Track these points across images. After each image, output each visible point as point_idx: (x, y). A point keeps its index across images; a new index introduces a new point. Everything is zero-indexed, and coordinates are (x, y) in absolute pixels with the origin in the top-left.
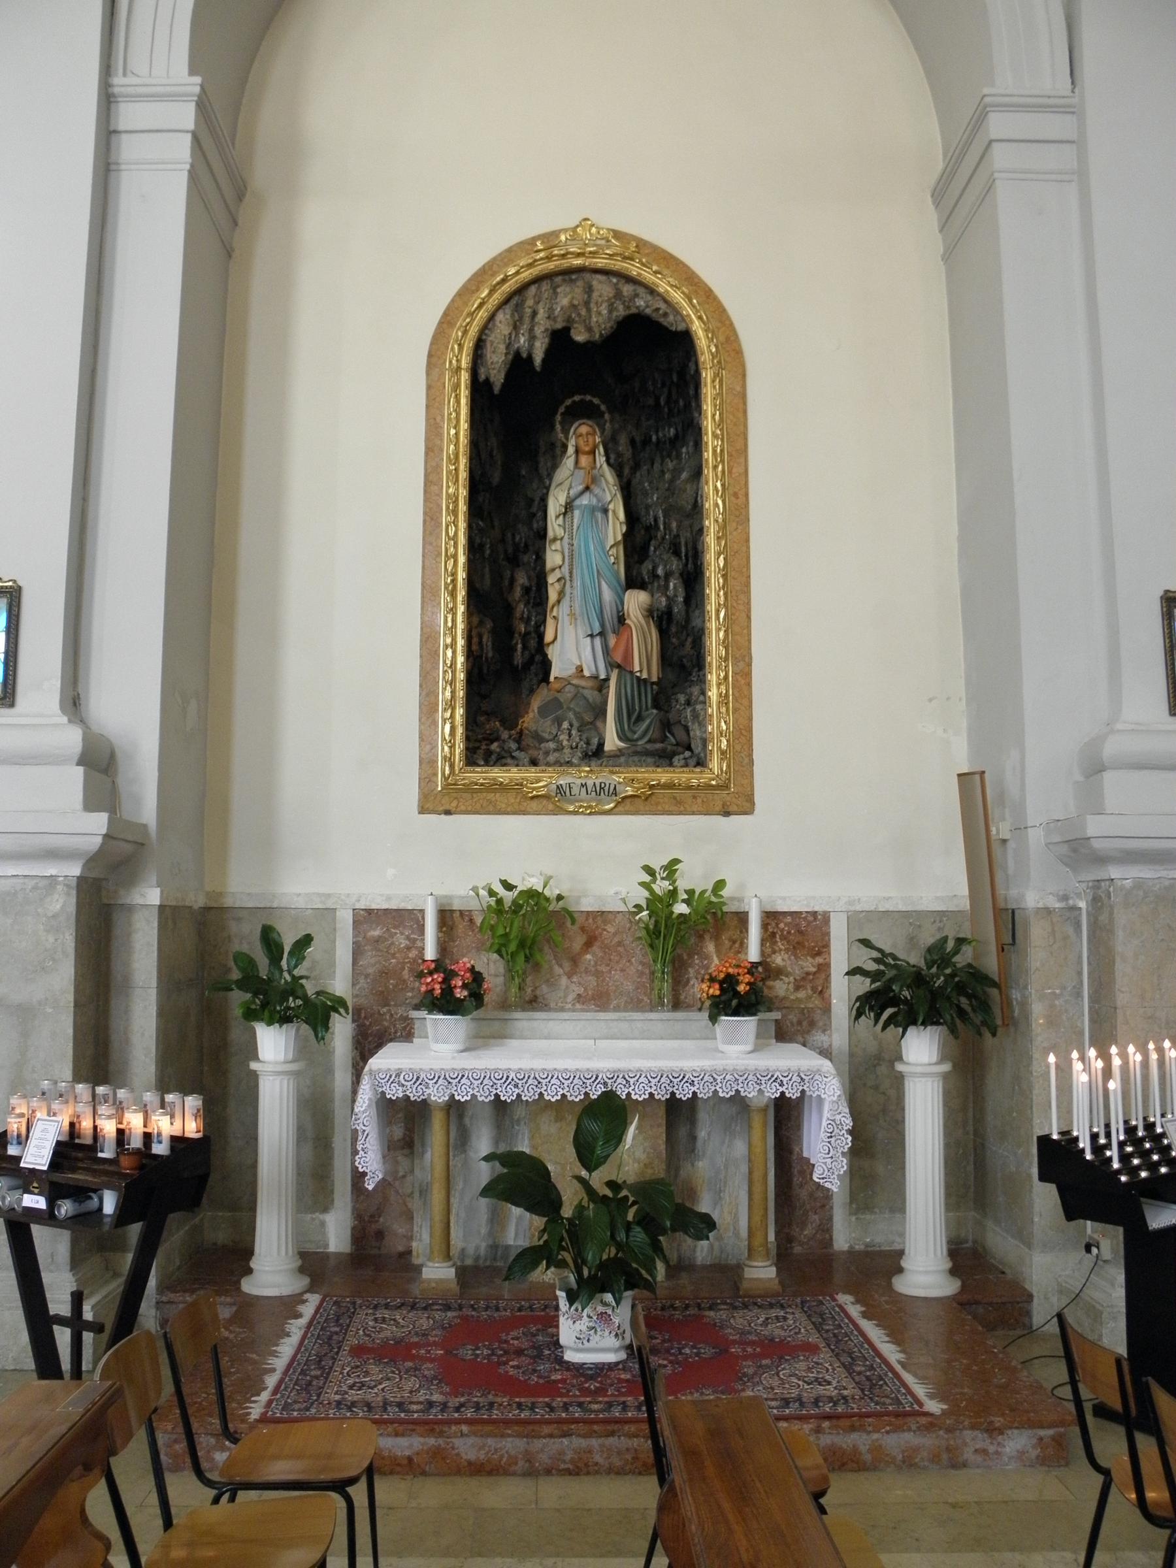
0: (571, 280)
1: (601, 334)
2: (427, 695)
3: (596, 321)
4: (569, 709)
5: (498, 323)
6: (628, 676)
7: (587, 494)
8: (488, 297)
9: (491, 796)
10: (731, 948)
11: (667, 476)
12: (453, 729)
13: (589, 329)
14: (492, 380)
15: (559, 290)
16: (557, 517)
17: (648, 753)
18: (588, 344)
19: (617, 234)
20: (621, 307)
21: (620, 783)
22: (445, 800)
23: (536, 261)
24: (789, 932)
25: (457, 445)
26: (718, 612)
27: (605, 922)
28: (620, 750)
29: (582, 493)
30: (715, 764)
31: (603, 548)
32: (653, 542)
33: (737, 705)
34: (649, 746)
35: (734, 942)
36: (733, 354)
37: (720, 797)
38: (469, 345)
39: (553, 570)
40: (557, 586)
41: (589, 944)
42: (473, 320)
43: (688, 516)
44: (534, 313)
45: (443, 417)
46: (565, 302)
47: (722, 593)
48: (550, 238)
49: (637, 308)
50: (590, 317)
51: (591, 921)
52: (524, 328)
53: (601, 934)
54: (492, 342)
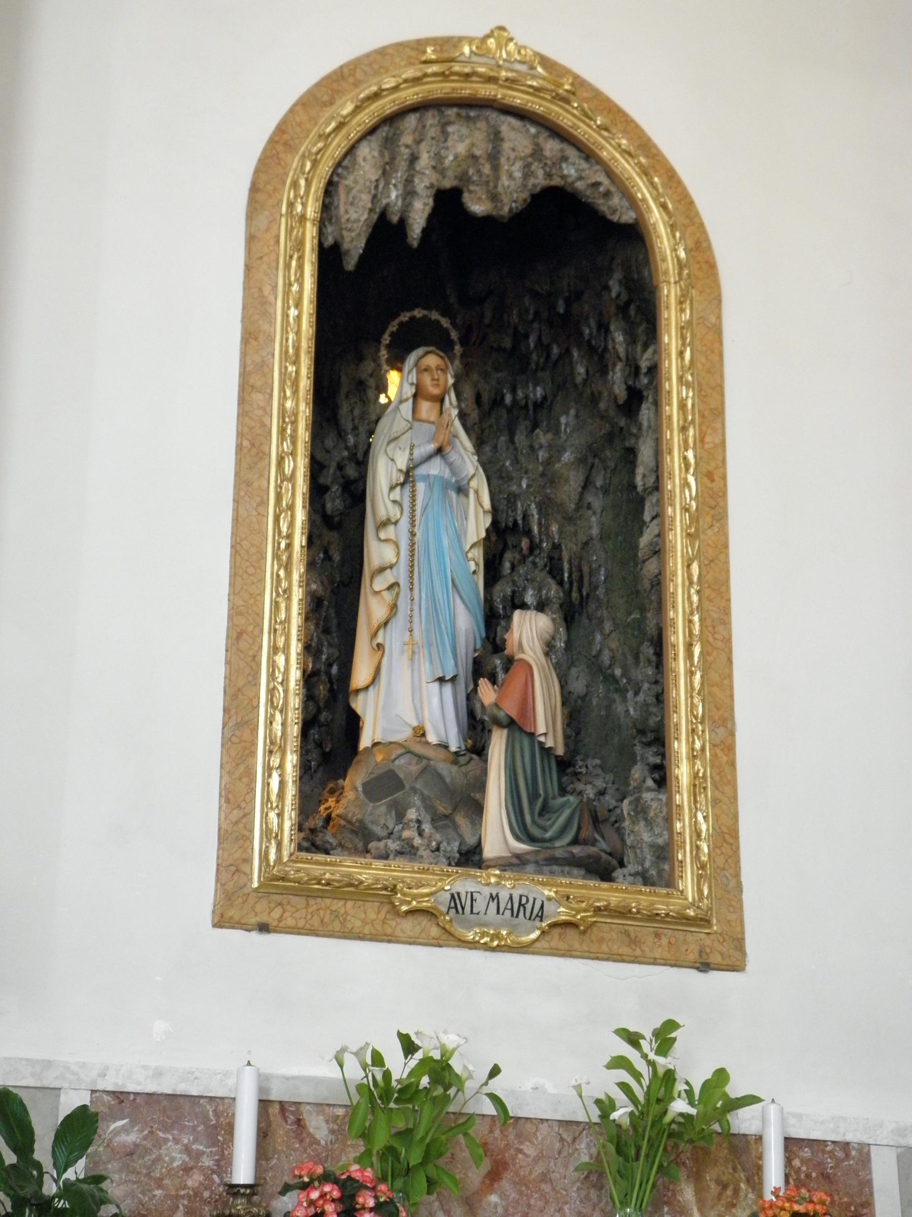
0: (468, 118)
1: (511, 209)
2: (238, 726)
3: (503, 189)
4: (414, 790)
5: (360, 159)
6: (526, 742)
7: (437, 461)
8: (352, 113)
9: (338, 905)
10: (719, 1197)
11: (542, 455)
12: (282, 784)
13: (494, 197)
14: (346, 246)
15: (450, 129)
16: (392, 488)
17: (573, 862)
18: (488, 220)
19: (545, 62)
20: (540, 173)
21: (549, 899)
22: (262, 905)
23: (426, 75)
24: (808, 1176)
25: (298, 333)
26: (689, 647)
27: (520, 1136)
28: (518, 856)
29: (429, 457)
30: (687, 883)
31: (461, 547)
32: (508, 555)
33: (718, 795)
34: (576, 850)
35: (725, 1187)
36: (705, 267)
37: (696, 938)
38: (318, 186)
39: (382, 570)
40: (388, 597)
41: (494, 1176)
42: (326, 147)
43: (570, 519)
44: (414, 159)
45: (275, 287)
46: (462, 148)
47: (696, 618)
48: (447, 45)
49: (563, 177)
50: (498, 178)
51: (497, 1133)
52: (400, 175)
53: (514, 1158)
54: (349, 190)
